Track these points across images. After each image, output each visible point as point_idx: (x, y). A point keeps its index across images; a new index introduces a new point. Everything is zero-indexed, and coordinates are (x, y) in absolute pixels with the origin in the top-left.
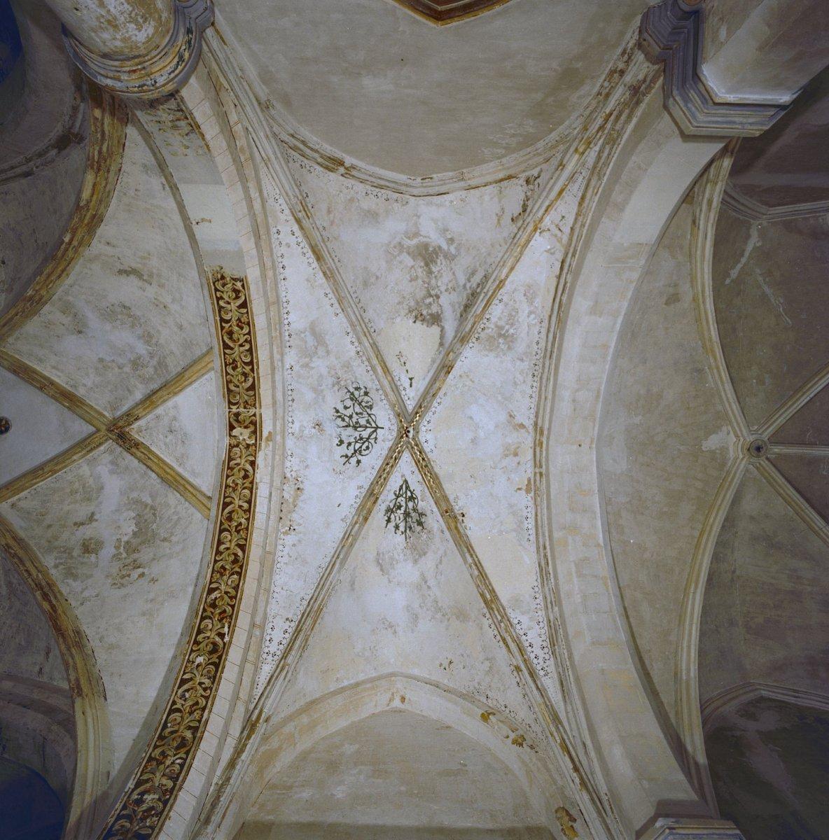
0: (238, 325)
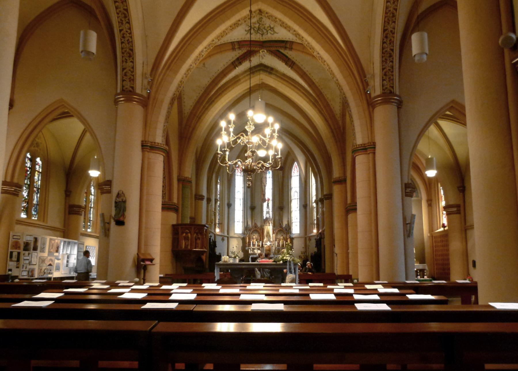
0: (127, 60)
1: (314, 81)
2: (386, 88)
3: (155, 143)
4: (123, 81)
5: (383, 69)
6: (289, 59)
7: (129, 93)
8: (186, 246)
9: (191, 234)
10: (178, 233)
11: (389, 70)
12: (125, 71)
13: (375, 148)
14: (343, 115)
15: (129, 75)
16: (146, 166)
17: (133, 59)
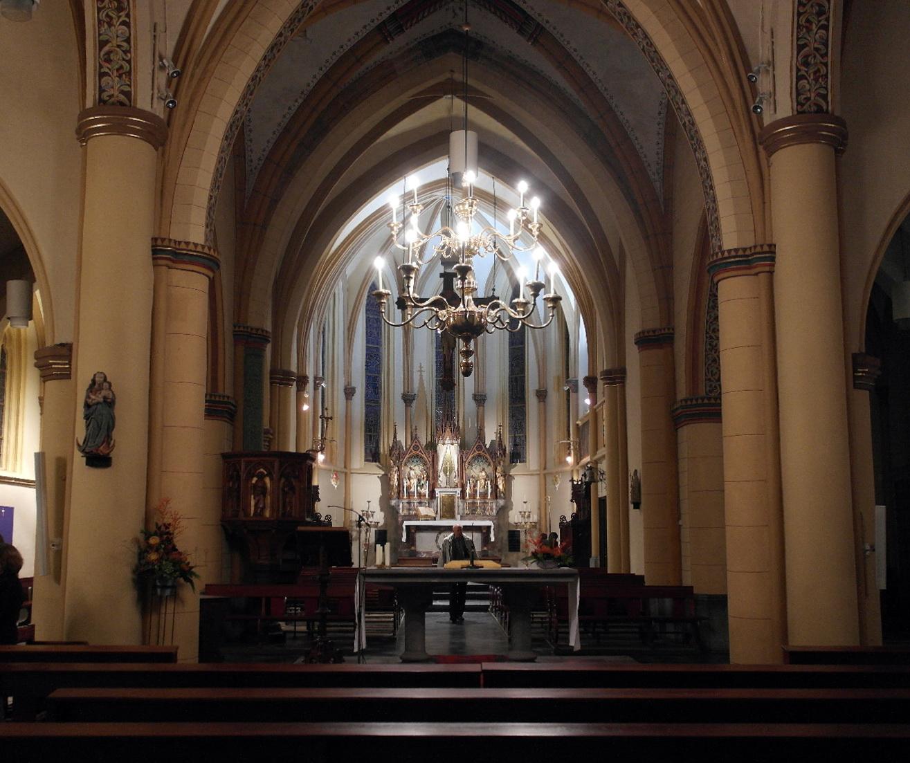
0: (111, 18)
1: (593, 78)
2: (808, 99)
3: (187, 243)
4: (102, 75)
5: (800, 48)
6: (528, 17)
7: (117, 111)
8: (260, 511)
9: (271, 479)
10: (239, 477)
11: (817, 49)
12: (106, 48)
13: (773, 259)
14: (669, 165)
15: (118, 62)
16: (162, 305)
17: (128, 15)
